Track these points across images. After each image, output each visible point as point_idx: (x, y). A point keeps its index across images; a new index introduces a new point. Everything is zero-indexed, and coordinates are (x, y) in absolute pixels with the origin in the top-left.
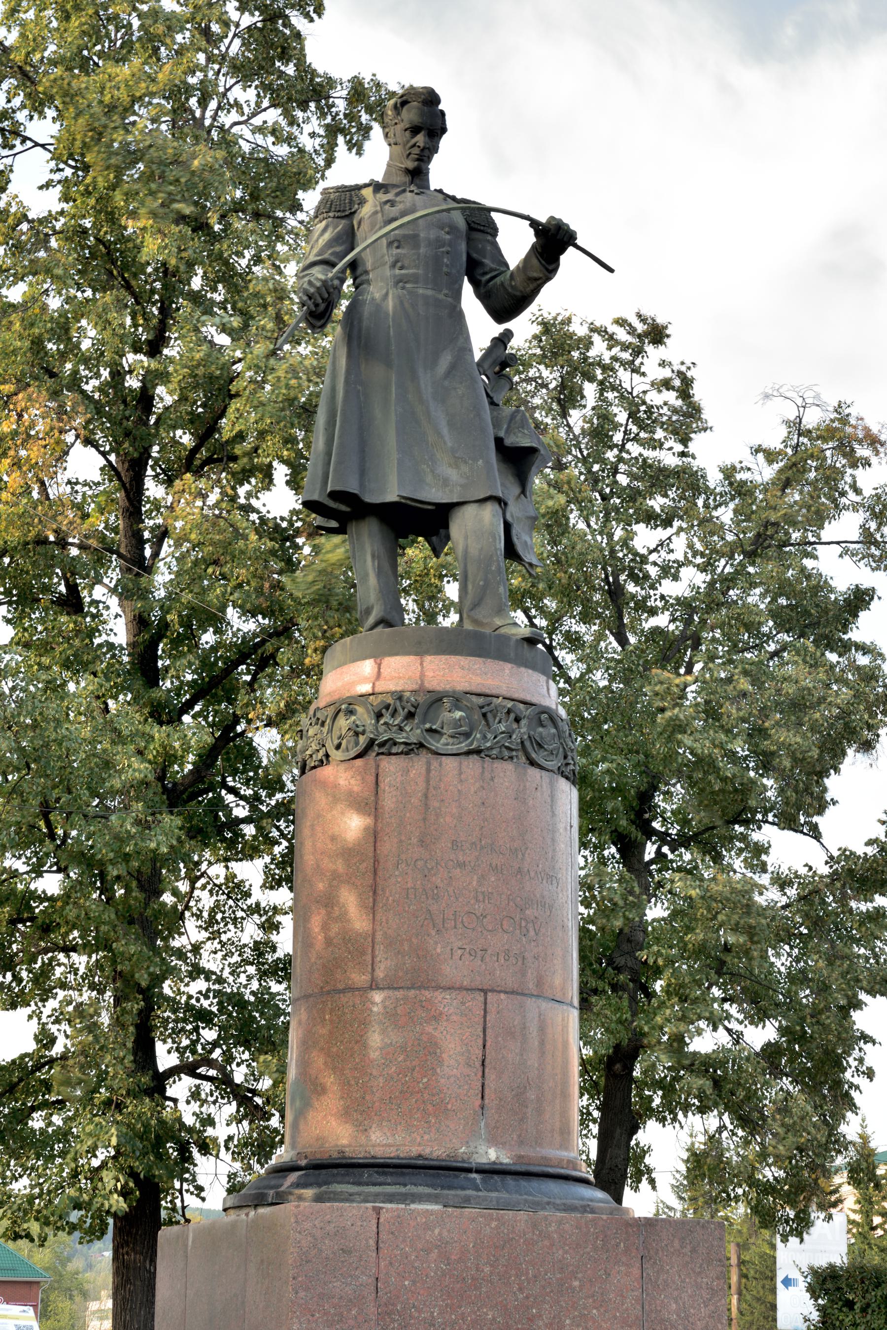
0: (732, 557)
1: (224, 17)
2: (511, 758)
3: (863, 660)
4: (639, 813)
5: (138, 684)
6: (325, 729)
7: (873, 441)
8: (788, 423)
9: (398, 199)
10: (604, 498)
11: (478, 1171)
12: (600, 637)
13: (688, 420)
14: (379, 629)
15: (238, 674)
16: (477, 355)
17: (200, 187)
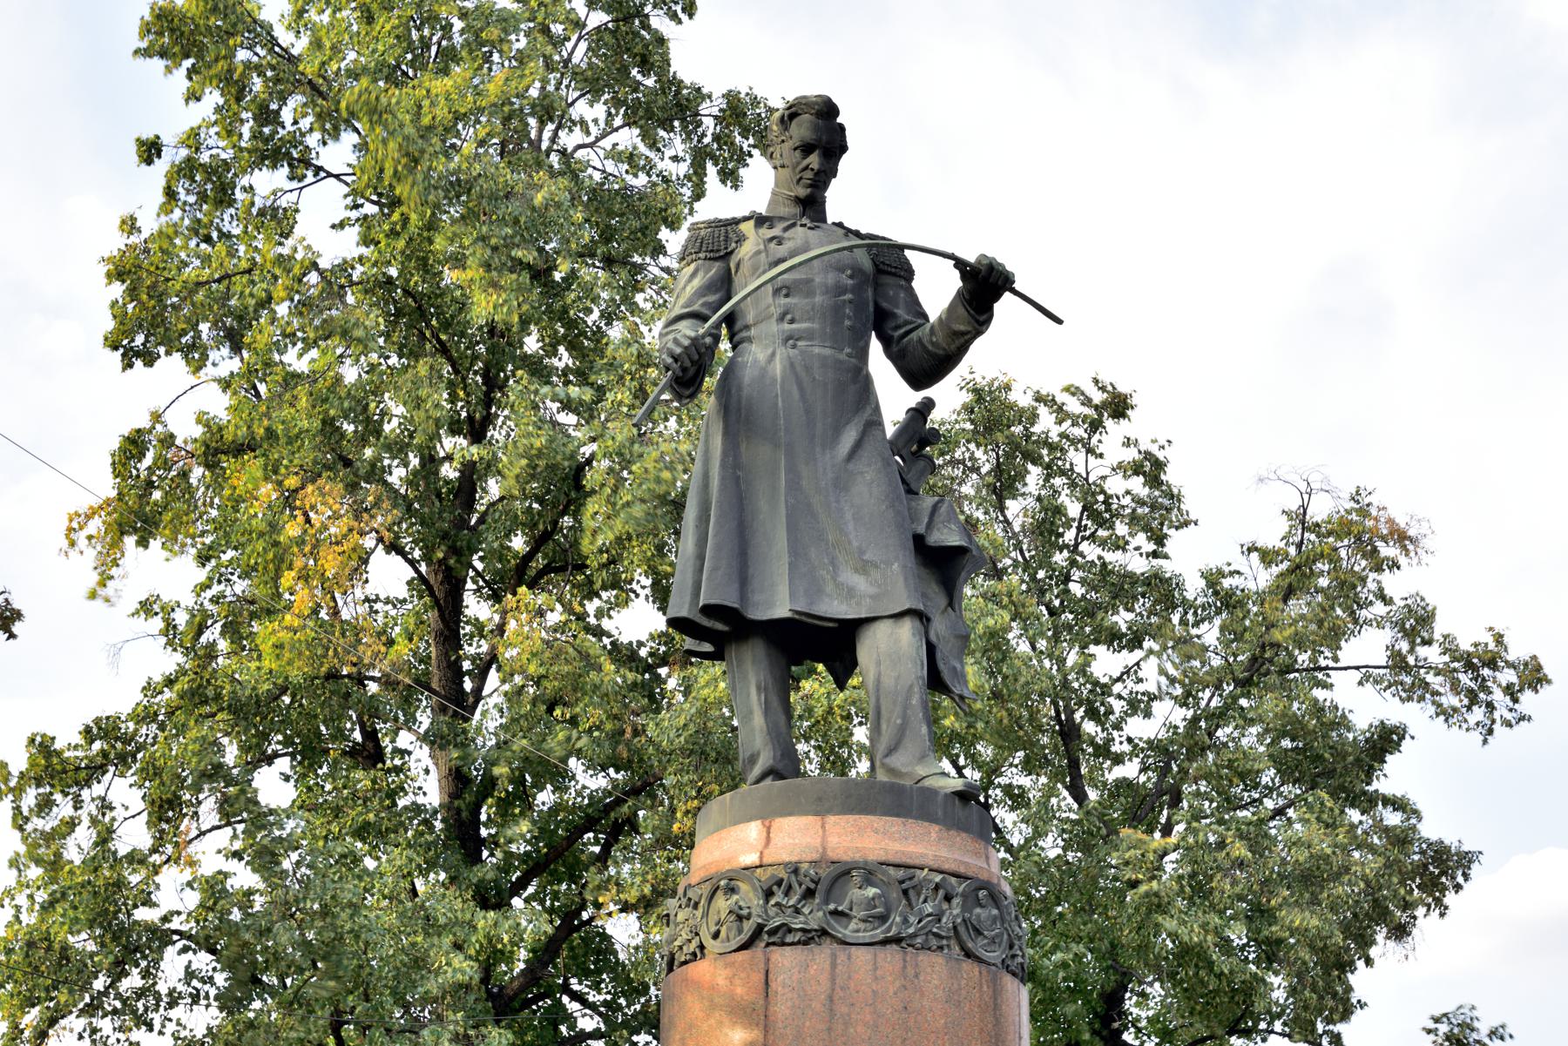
0: (1218, 687)
1: (572, 16)
2: (941, 948)
3: (1393, 818)
4: (1106, 1020)
5: (456, 857)
6: (699, 913)
7: (1401, 538)
9: (786, 235)
10: (1052, 612)
12: (1050, 792)
13: (1161, 513)
14: (768, 782)
15: (584, 844)
16: (890, 431)
17: (538, 224)
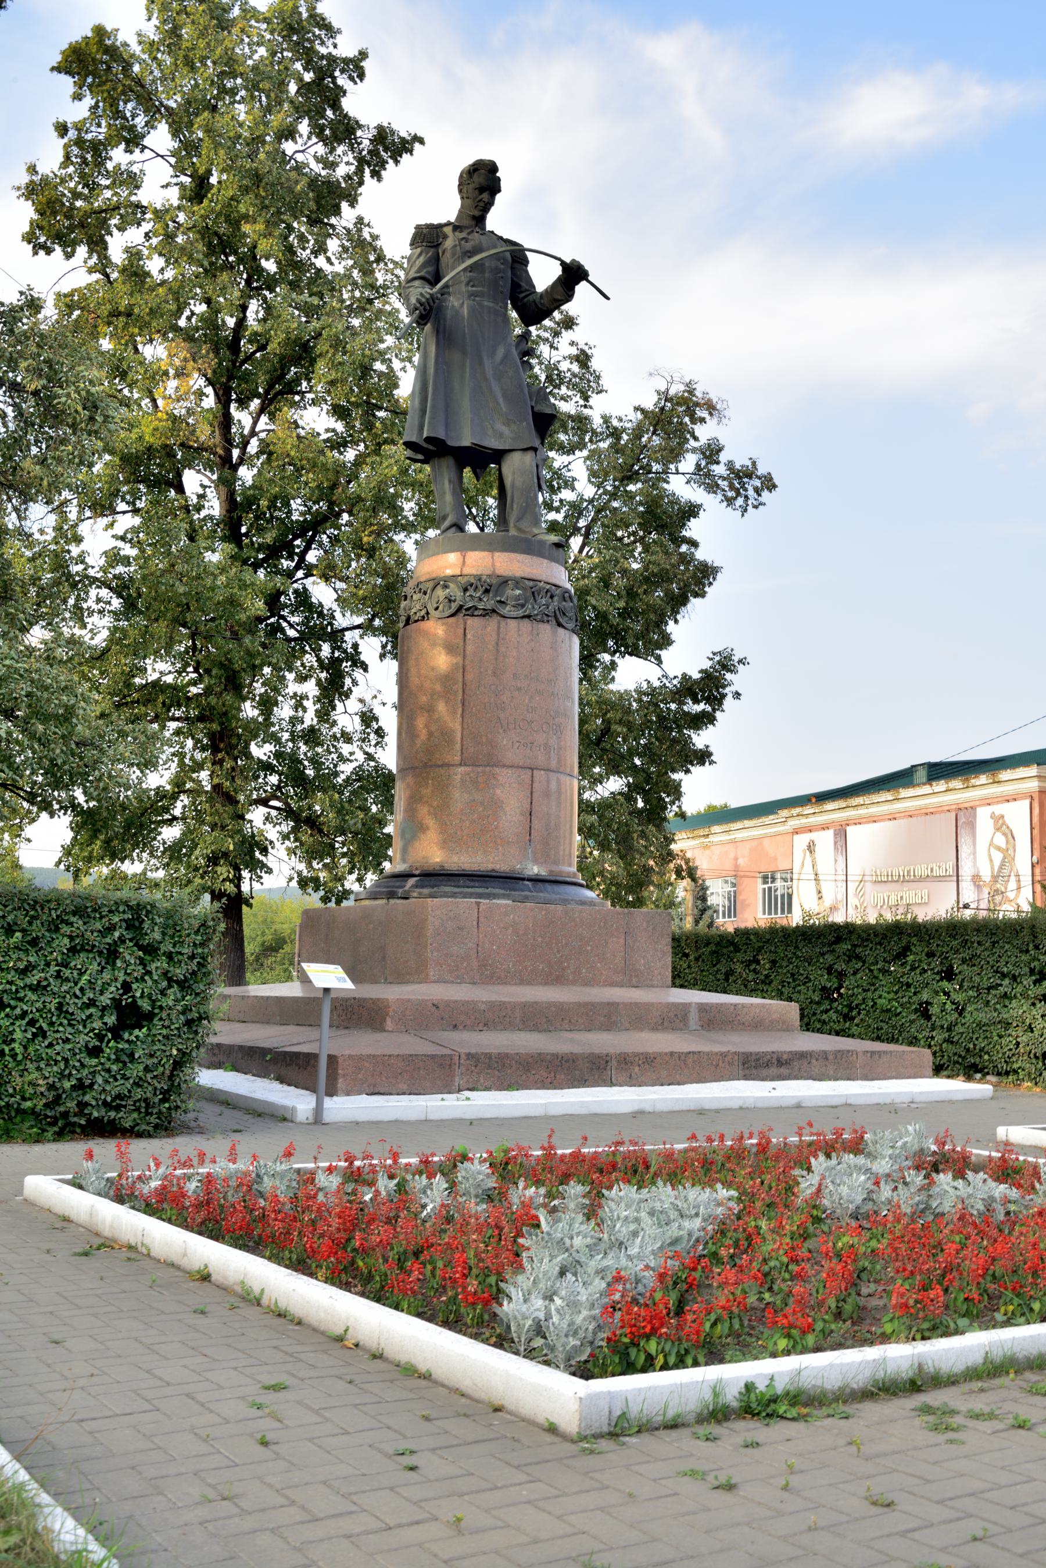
7: (711, 407)
8: (658, 392)
11: (529, 880)
13: (587, 383)
